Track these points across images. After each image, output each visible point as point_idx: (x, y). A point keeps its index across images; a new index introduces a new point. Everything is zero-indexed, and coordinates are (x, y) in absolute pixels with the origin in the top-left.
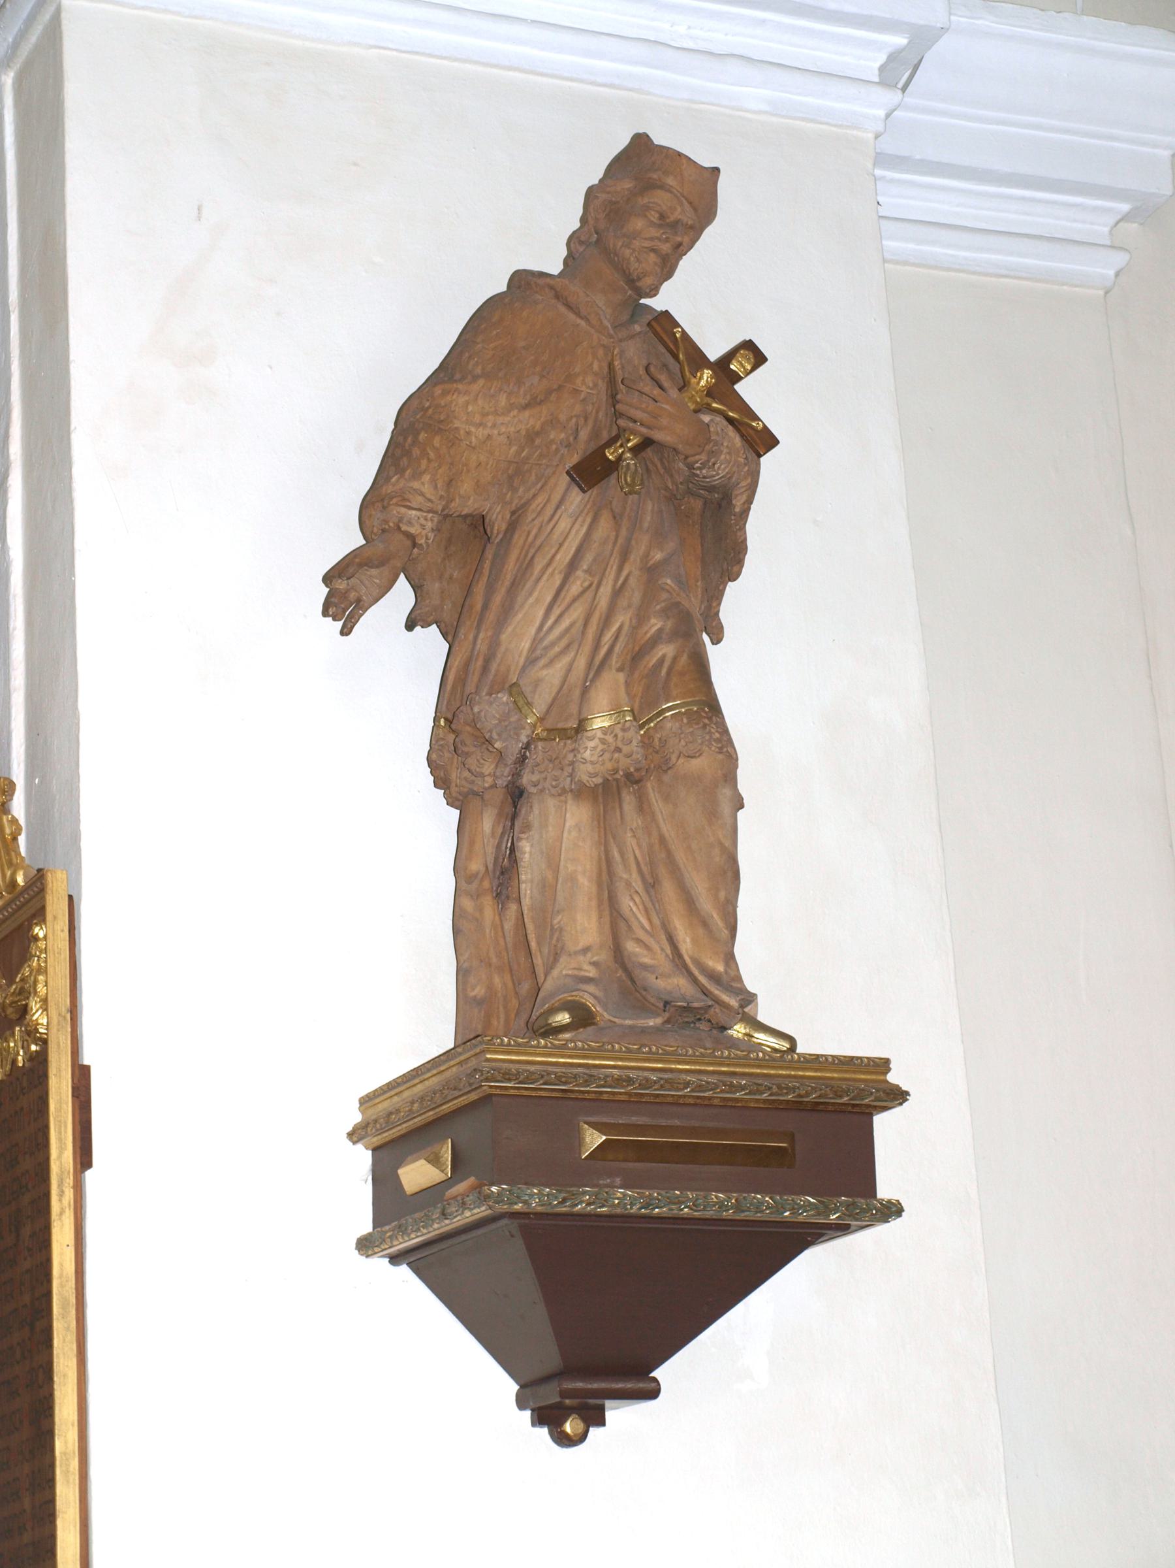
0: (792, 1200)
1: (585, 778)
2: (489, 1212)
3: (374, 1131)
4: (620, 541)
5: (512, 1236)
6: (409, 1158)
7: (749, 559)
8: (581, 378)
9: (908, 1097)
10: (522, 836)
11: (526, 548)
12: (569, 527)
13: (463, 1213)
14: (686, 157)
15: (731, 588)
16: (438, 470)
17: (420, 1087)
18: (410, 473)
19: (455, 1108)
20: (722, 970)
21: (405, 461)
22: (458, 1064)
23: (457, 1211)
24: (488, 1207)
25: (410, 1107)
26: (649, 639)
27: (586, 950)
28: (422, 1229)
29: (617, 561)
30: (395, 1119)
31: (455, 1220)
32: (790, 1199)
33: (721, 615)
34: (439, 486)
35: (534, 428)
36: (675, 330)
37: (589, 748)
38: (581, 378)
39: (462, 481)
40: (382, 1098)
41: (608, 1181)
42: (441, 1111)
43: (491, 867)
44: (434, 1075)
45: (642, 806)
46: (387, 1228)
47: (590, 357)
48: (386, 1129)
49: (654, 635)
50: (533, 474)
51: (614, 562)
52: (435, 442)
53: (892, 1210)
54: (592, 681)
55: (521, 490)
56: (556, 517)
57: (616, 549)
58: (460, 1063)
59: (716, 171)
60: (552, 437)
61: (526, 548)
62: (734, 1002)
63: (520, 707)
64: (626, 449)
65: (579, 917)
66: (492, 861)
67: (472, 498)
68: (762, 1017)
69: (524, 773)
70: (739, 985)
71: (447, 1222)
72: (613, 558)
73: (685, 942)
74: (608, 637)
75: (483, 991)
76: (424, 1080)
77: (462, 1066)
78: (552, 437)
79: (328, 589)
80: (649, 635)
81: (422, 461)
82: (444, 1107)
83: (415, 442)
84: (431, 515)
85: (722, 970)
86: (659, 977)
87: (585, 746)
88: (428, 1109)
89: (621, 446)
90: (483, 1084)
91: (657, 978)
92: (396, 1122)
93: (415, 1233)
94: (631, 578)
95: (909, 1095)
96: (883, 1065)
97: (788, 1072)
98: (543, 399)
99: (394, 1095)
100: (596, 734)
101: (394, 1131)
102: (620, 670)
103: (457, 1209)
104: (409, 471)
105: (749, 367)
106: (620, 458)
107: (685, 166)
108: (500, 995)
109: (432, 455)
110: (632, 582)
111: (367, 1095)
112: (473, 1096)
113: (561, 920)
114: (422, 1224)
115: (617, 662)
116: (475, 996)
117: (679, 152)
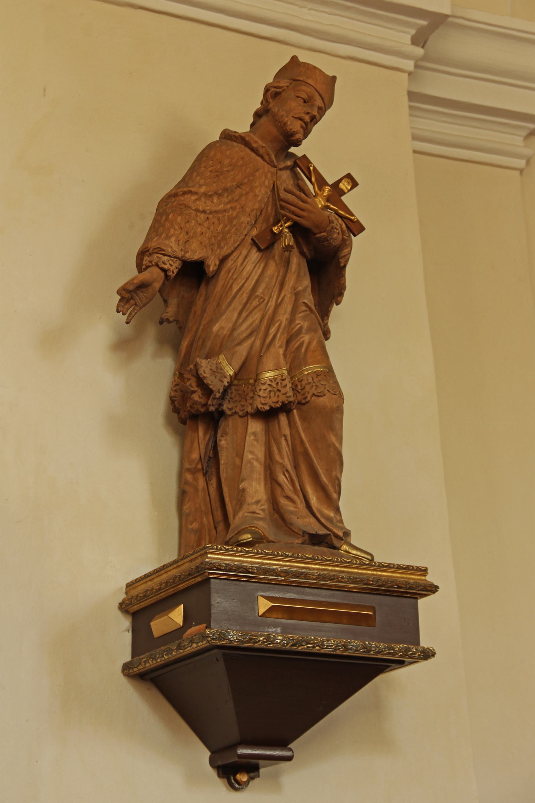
0: (375, 645)
1: (260, 406)
2: (208, 644)
3: (136, 601)
4: (280, 278)
5: (218, 660)
6: (157, 616)
7: (346, 293)
8: (259, 189)
9: (438, 589)
10: (222, 439)
11: (228, 280)
12: (252, 269)
13: (191, 645)
14: (319, 69)
15: (335, 309)
16: (179, 235)
17: (165, 576)
18: (164, 236)
19: (186, 586)
20: (333, 516)
21: (161, 229)
22: (190, 561)
23: (188, 644)
24: (207, 642)
25: (160, 586)
26: (295, 332)
27: (258, 502)
28: (165, 656)
29: (277, 288)
30: (150, 593)
31: (186, 650)
32: (374, 644)
33: (329, 324)
34: (180, 244)
35: (232, 215)
36: (310, 165)
37: (262, 390)
38: (259, 189)
39: (192, 242)
40: (141, 583)
41: (273, 629)
42: (177, 589)
43: (202, 456)
44: (174, 568)
45: (291, 424)
46: (143, 656)
47: (263, 178)
48: (144, 600)
49: (298, 329)
50: (232, 239)
51: (276, 288)
52: (178, 219)
53: (428, 654)
54: (264, 353)
55: (225, 248)
56: (245, 263)
57: (278, 282)
58: (191, 561)
59: (334, 78)
60: (242, 220)
61: (228, 280)
62: (341, 534)
63: (224, 366)
64: (284, 227)
65: (254, 483)
66: (204, 453)
67: (198, 252)
68: (353, 542)
69: (224, 403)
70: (341, 525)
71: (181, 651)
72: (275, 287)
73: (313, 499)
74: (272, 331)
75: (197, 525)
76: (168, 571)
77: (192, 562)
78: (242, 220)
79: (120, 297)
80: (295, 330)
81: (171, 230)
82: (180, 586)
83: (167, 219)
84: (175, 259)
85: (333, 516)
86: (299, 518)
87: (260, 388)
88: (171, 587)
89: (281, 226)
90: (206, 571)
91: (298, 518)
92: (151, 595)
93: (159, 659)
94: (285, 298)
95: (439, 588)
96: (424, 571)
97: (372, 572)
98: (237, 199)
99: (149, 581)
100: (266, 382)
101: (148, 601)
102: (280, 347)
103: (188, 643)
104: (164, 234)
105: (349, 188)
106: (281, 232)
107: (318, 74)
108: (206, 528)
109: (177, 227)
110: (286, 300)
111: (131, 582)
112: (199, 579)
113: (244, 485)
114: (165, 653)
115: (278, 343)
116: (192, 528)
117: (315, 66)
